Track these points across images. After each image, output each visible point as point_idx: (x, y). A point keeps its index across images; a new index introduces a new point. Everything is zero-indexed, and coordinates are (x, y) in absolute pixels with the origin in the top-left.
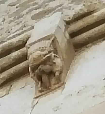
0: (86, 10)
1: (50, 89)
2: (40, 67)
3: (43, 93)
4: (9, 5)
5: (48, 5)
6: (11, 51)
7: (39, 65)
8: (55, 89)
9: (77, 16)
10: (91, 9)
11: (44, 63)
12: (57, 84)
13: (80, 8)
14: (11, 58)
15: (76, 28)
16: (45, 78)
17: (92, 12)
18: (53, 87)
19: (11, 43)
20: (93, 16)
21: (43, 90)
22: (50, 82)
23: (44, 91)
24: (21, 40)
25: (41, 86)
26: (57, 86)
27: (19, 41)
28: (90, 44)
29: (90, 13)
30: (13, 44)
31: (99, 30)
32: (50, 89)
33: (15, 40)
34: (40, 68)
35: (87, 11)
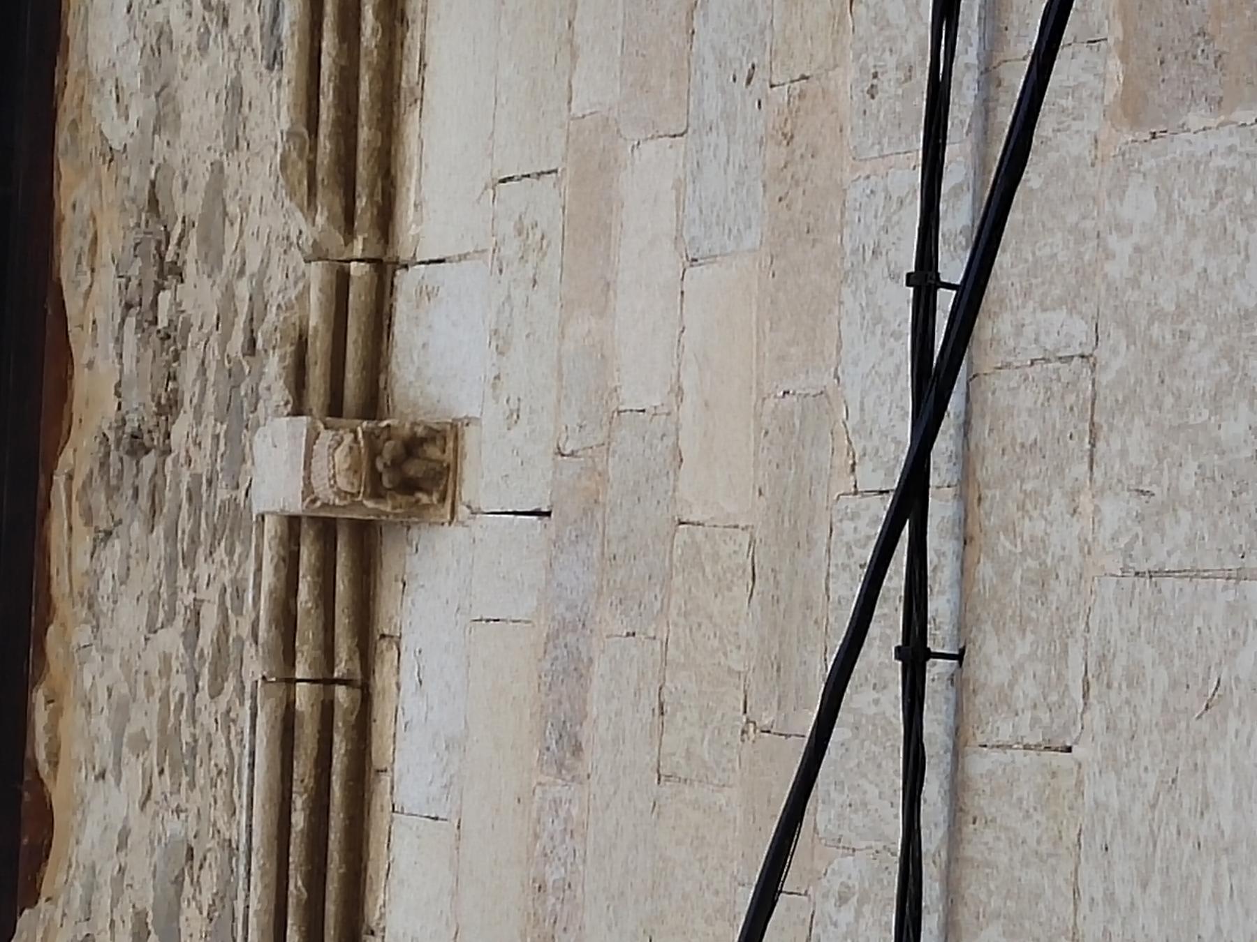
0: (290, 349)
1: (448, 467)
2: (380, 466)
3: (450, 492)
4: (143, 806)
5: (202, 650)
6: (289, 611)
7: (373, 467)
8: (456, 450)
9: (291, 379)
10: (294, 334)
11: (374, 453)
12: (445, 443)
13: (276, 358)
14: (309, 611)
15: (322, 391)
16: (414, 469)
17: (300, 337)
18: (449, 457)
19: (271, 593)
20: (315, 328)
21: (441, 487)
22: (430, 460)
23: (446, 486)
24: (275, 560)
25: (430, 493)
26: (450, 445)
27: (276, 568)
28: (382, 378)
29: (302, 345)
30: (276, 588)
31: (359, 330)
32: (448, 467)
33: (268, 578)
34: (385, 465)
35: (293, 348)
